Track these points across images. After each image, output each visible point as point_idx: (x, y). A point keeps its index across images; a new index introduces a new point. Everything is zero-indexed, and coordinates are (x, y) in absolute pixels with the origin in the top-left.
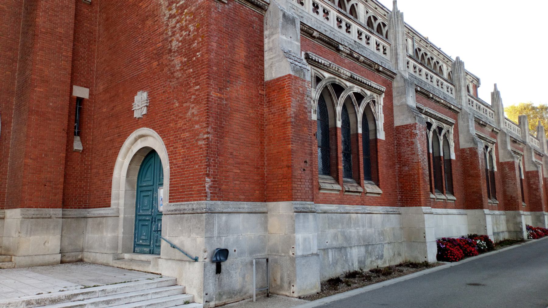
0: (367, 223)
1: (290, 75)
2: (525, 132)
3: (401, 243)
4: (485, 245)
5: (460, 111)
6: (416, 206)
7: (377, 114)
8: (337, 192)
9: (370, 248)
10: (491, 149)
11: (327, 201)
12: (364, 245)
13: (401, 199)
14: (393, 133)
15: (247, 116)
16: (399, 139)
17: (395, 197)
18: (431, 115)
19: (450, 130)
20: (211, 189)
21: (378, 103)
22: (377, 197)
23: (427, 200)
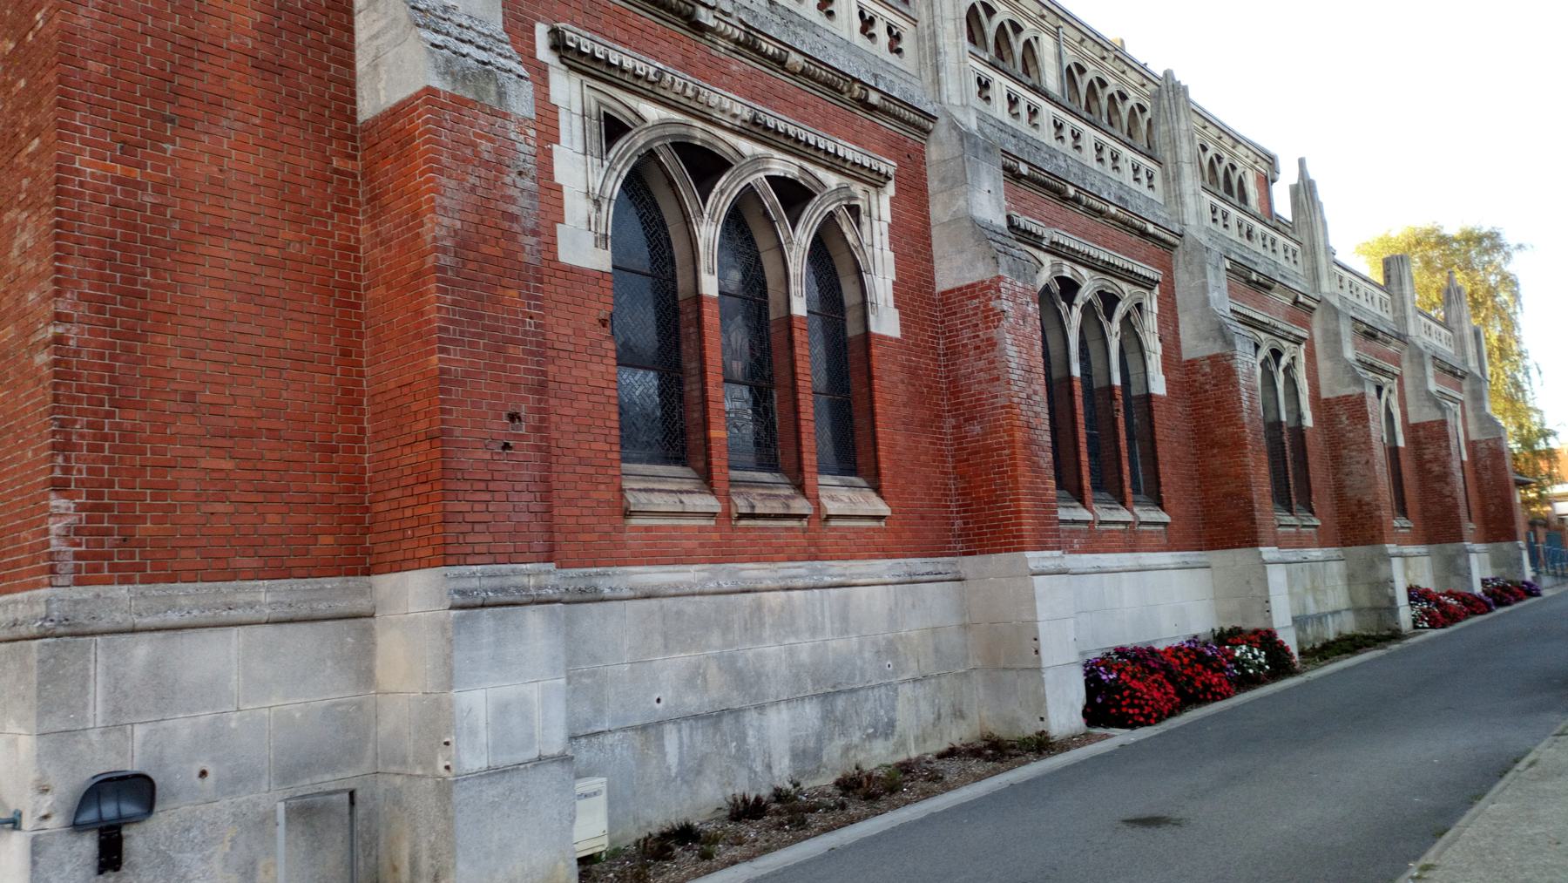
0: (827, 621)
1: (430, 91)
2: (1404, 304)
3: (965, 674)
4: (1263, 661)
5: (1177, 242)
6: (1007, 551)
7: (869, 251)
8: (703, 522)
9: (840, 703)
10: (1293, 358)
11: (662, 554)
12: (817, 696)
13: (962, 530)
14: (933, 316)
15: (271, 251)
16: (951, 334)
17: (937, 524)
18: (1073, 256)
19: (1146, 302)
20: (77, 539)
21: (870, 216)
22: (873, 529)
23: (1047, 530)
